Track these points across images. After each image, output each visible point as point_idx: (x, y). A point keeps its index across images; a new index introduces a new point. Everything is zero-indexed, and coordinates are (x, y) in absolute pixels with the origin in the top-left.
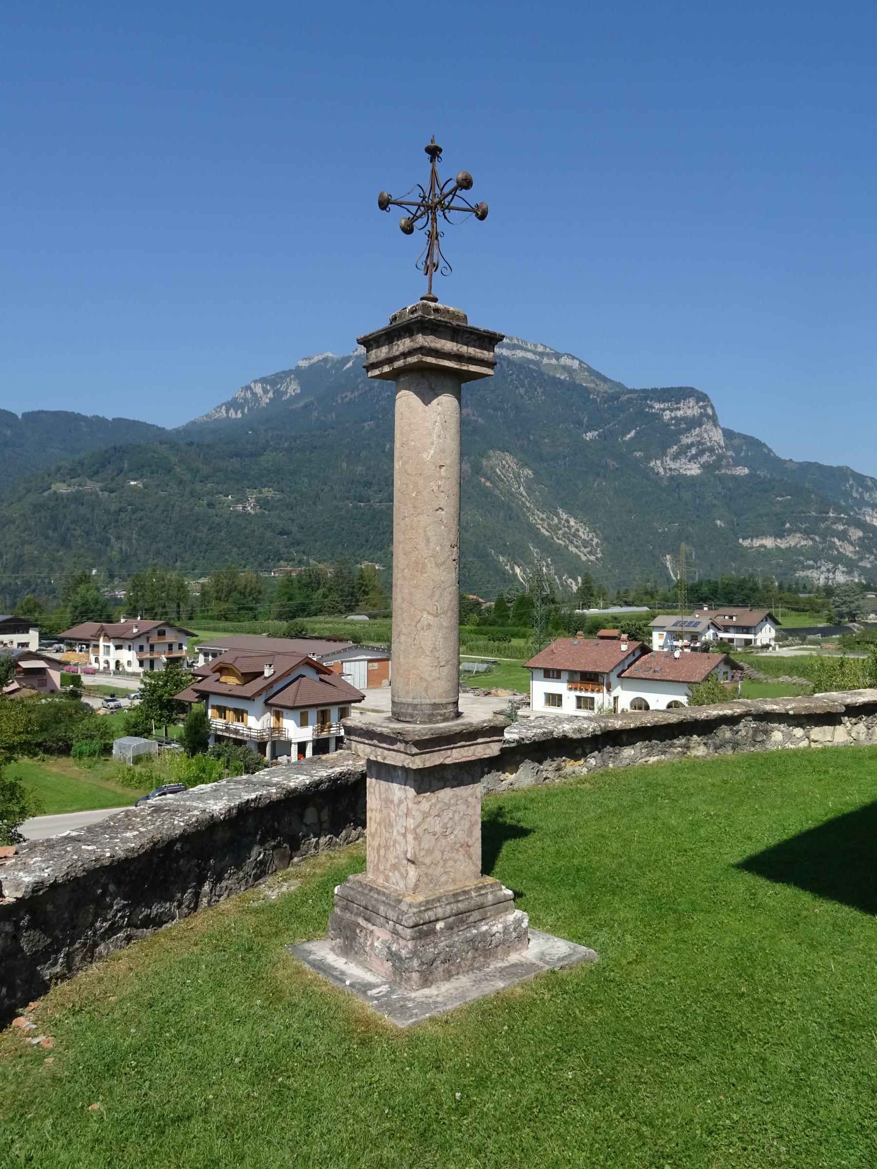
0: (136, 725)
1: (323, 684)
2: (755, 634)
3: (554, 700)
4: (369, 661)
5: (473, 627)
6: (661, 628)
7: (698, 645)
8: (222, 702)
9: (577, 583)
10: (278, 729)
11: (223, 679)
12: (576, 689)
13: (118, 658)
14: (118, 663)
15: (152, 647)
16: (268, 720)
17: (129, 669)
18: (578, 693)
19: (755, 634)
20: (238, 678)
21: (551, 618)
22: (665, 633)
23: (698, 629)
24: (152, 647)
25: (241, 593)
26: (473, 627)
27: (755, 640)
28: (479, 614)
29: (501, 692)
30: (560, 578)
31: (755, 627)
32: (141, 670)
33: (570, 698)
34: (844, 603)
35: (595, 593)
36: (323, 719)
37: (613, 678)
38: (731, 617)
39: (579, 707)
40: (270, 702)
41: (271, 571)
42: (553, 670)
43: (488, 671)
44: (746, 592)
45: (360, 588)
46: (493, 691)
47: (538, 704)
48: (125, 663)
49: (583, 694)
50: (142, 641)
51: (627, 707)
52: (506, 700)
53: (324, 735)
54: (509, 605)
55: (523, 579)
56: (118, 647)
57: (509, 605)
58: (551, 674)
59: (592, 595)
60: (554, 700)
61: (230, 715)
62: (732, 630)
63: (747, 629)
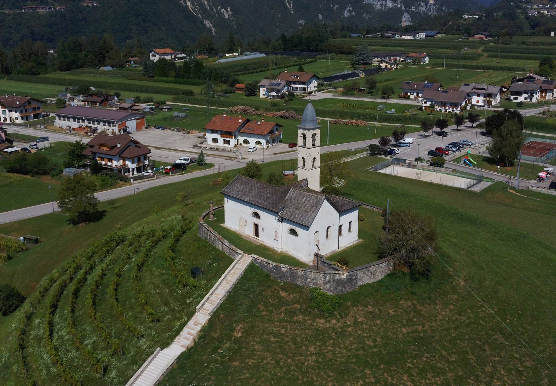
0: (69, 163)
1: (136, 148)
2: (308, 85)
3: (215, 140)
4: (137, 119)
5: (173, 79)
6: (263, 86)
7: (280, 95)
8: (103, 156)
9: (227, 12)
10: (124, 165)
11: (102, 148)
12: (223, 137)
13: (10, 116)
14: (10, 118)
15: (26, 111)
16: (121, 162)
17: (17, 121)
18: (224, 139)
19: (308, 85)
20: (108, 148)
21: (212, 74)
22: (265, 89)
23: (280, 87)
24: (26, 111)
25: (36, 55)
26: (173, 79)
27: (307, 88)
28: (175, 71)
29: (194, 132)
30: (216, 8)
31: (307, 82)
32: (23, 121)
33: (221, 140)
34: (361, 54)
35: (236, 44)
36: (139, 161)
37: (237, 133)
38: (297, 77)
39: (224, 143)
40: (121, 156)
41: (22, 9)
42: (215, 130)
43: (186, 116)
44: (317, 42)
45: (104, 49)
46: (191, 132)
47: (210, 142)
48: (15, 118)
49: (226, 139)
50: (22, 108)
51: (242, 142)
52: (196, 136)
53: (140, 165)
54: (190, 66)
55: (192, 9)
56: (10, 111)
57: (190, 66)
58: (214, 131)
59: (234, 45)
60: (215, 140)
61: (106, 160)
62: (297, 83)
63: (303, 83)
